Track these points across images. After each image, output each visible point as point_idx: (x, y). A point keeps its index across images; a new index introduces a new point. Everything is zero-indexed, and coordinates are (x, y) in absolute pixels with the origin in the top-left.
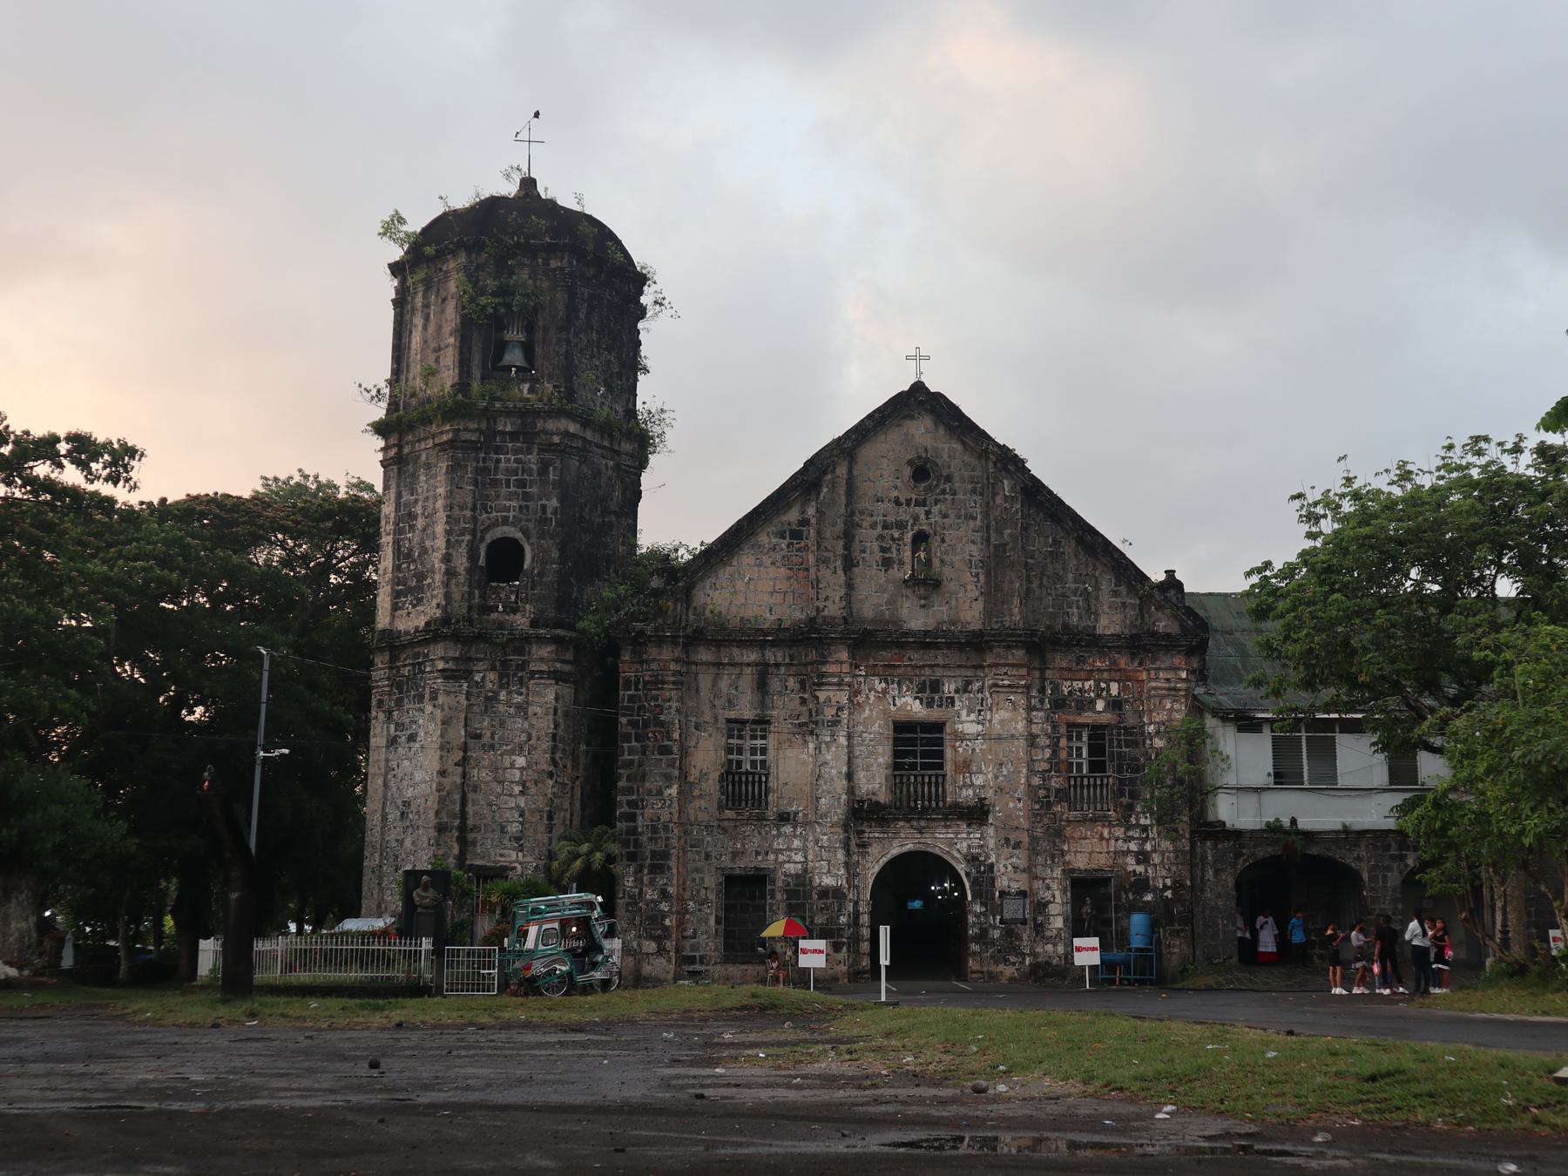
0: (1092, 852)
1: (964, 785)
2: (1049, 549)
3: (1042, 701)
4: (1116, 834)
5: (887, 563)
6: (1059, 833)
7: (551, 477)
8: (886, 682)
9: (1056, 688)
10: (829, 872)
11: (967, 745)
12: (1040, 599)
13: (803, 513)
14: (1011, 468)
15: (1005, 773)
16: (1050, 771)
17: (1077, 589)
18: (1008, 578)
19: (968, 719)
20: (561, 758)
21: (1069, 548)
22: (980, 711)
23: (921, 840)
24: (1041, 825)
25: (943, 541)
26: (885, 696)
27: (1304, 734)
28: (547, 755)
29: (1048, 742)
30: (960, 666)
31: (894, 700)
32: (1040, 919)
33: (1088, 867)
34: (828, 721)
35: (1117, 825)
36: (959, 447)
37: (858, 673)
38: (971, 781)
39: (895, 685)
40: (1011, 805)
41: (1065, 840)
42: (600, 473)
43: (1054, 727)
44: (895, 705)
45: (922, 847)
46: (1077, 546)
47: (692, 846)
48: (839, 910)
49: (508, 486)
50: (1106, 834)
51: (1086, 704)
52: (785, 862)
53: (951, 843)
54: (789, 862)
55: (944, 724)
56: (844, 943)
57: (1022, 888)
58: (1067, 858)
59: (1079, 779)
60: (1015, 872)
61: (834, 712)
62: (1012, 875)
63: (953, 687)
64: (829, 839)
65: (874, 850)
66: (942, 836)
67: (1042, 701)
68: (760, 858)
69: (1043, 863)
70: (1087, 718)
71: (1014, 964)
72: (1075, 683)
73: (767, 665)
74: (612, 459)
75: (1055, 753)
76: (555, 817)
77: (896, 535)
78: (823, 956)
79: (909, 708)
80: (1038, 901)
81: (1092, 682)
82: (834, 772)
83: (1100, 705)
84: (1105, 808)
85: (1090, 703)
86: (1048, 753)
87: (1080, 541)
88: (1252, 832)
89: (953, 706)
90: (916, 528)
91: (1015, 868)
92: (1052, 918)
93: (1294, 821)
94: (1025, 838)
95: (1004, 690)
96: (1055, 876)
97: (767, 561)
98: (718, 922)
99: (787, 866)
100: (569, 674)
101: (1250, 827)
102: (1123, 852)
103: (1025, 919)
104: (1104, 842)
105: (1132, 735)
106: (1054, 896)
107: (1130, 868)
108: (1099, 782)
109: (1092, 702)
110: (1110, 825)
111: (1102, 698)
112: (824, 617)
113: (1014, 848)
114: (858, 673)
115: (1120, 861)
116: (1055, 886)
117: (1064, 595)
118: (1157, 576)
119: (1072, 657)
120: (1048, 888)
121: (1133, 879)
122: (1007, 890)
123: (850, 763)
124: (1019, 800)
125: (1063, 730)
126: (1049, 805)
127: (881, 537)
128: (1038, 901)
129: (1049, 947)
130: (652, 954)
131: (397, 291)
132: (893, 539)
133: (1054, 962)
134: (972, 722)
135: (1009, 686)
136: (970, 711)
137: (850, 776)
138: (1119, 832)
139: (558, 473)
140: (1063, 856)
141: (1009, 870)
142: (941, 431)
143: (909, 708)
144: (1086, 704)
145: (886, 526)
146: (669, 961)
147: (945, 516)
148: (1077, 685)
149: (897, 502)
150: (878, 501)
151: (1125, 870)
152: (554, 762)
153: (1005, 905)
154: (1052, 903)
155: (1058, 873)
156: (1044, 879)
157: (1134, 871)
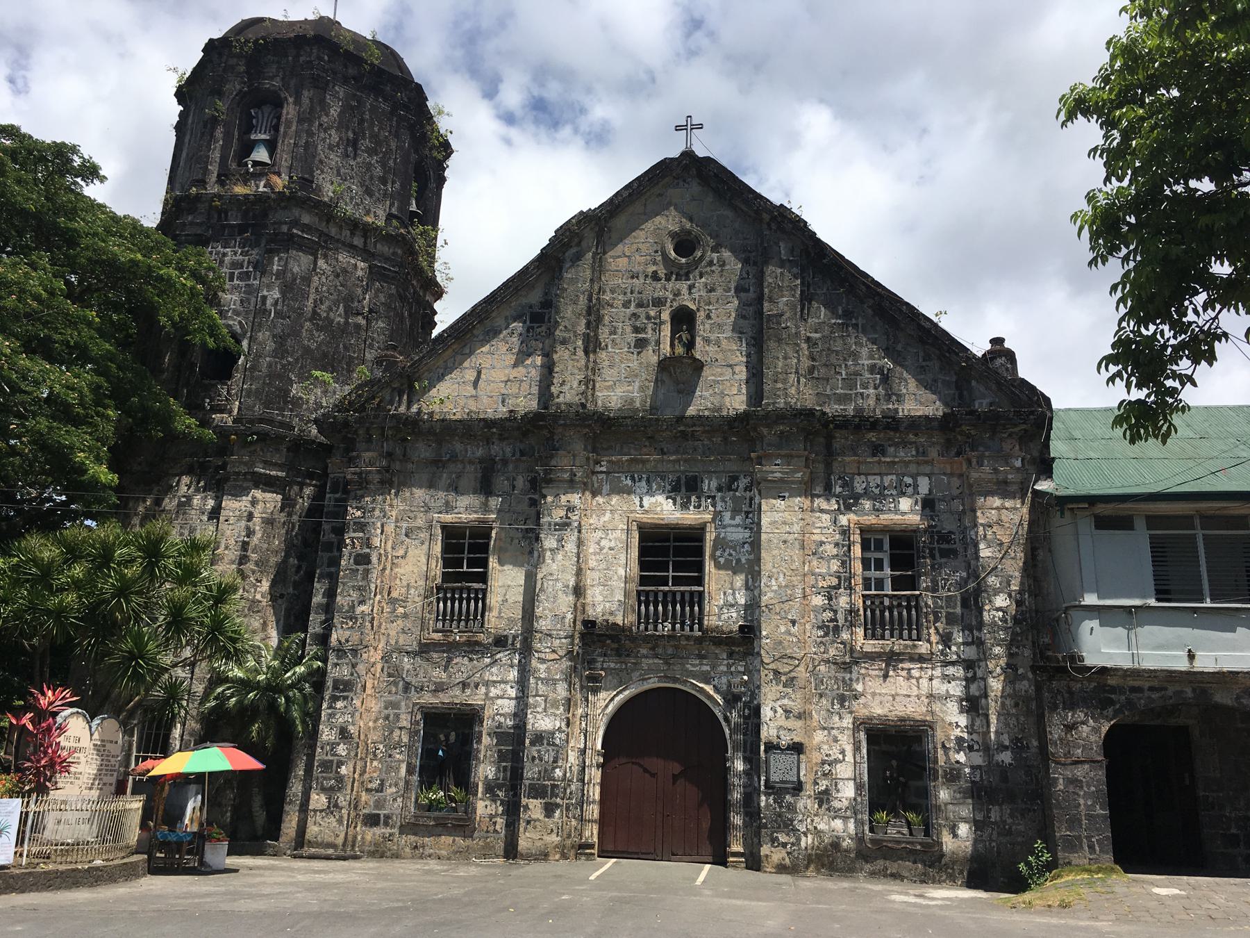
5: (641, 344)
7: (275, 267)
11: (730, 555)
13: (546, 294)
19: (733, 522)
22: (747, 513)
25: (708, 317)
27: (1200, 533)
28: (234, 566)
29: (835, 551)
34: (556, 524)
36: (729, 213)
37: (598, 469)
39: (644, 483)
44: (642, 506)
48: (555, 761)
49: (231, 279)
52: (498, 697)
54: (502, 697)
56: (558, 806)
57: (796, 739)
59: (914, 637)
60: (787, 718)
61: (563, 513)
62: (782, 721)
63: (714, 484)
64: (548, 668)
68: (468, 692)
72: (870, 478)
73: (492, 460)
77: (652, 313)
82: (559, 585)
84: (914, 637)
90: (675, 304)
91: (787, 712)
98: (410, 771)
99: (499, 702)
105: (948, 542)
106: (843, 752)
112: (558, 405)
114: (598, 469)
117: (857, 374)
118: (979, 346)
122: (775, 741)
123: (579, 572)
126: (837, 630)
127: (635, 316)
130: (321, 811)
131: (181, 114)
132: (648, 318)
133: (845, 844)
134: (737, 526)
136: (735, 512)
137: (578, 591)
139: (282, 263)
141: (778, 715)
142: (710, 199)
145: (640, 305)
146: (340, 821)
147: (712, 290)
150: (632, 277)
153: (772, 762)
155: (848, 721)
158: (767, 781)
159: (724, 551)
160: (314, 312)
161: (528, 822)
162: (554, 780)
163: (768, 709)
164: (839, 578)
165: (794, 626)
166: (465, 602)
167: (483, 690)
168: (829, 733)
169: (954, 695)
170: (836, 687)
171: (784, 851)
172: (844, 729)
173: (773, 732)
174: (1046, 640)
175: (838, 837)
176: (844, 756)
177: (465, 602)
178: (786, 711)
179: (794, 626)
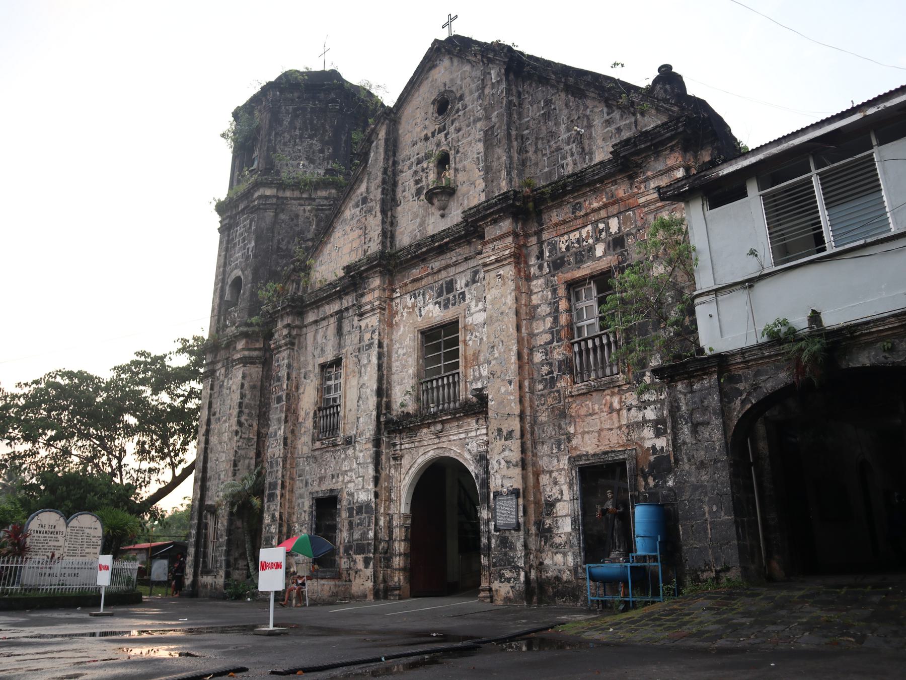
0: (601, 430)
1: (474, 379)
2: (542, 112)
3: (541, 267)
4: (628, 403)
6: (563, 414)
8: (415, 297)
9: (554, 247)
10: (363, 488)
12: (536, 164)
14: (491, 55)
15: (497, 355)
16: (551, 342)
17: (569, 138)
18: (496, 156)
20: (247, 420)
21: (560, 100)
23: (440, 445)
24: (544, 407)
26: (413, 310)
30: (466, 259)
31: (420, 310)
32: (548, 522)
33: (598, 450)
35: (628, 390)
38: (480, 373)
40: (503, 390)
41: (573, 420)
42: (297, 216)
43: (554, 291)
45: (440, 453)
46: (567, 96)
47: (299, 477)
50: (616, 405)
51: (584, 254)
53: (464, 444)
55: (457, 322)
57: (515, 487)
58: (574, 442)
59: (583, 343)
60: (508, 467)
62: (505, 471)
65: (405, 462)
66: (455, 438)
67: (541, 267)
69: (549, 452)
70: (586, 269)
71: (509, 580)
72: (572, 236)
74: (309, 205)
75: (556, 320)
76: (240, 464)
78: (281, 572)
79: (431, 315)
80: (546, 500)
81: (589, 228)
83: (600, 250)
85: (589, 251)
86: (549, 322)
87: (568, 89)
88: (743, 352)
89: (464, 300)
92: (560, 520)
93: (815, 317)
94: (516, 425)
95: (492, 267)
96: (562, 466)
97: (348, 228)
100: (257, 358)
101: (742, 344)
102: (637, 423)
103: (518, 524)
104: (615, 415)
106: (561, 493)
107: (648, 444)
108: (605, 341)
109: (591, 249)
110: (621, 392)
111: (602, 241)
113: (506, 439)
115: (635, 436)
116: (562, 479)
119: (568, 209)
120: (556, 483)
121: (652, 458)
122: (500, 489)
124: (510, 382)
125: (562, 292)
126: (553, 381)
128: (546, 500)
129: (559, 558)
135: (497, 261)
138: (631, 398)
140: (569, 440)
141: (502, 466)
143: (431, 315)
144: (584, 254)
148: (575, 236)
149: (426, 138)
151: (641, 447)
152: (240, 424)
154: (559, 500)
155: (564, 462)
156: (551, 472)
157: (654, 447)
158: (495, 525)
159: (472, 335)
160: (278, 248)
161: (356, 572)
162: (369, 540)
163: (495, 462)
164: (552, 333)
165: (510, 385)
166: (441, 389)
167: (341, 479)
168: (550, 476)
169: (650, 421)
170: (553, 433)
171: (509, 585)
172: (561, 470)
173: (499, 482)
174: (563, 384)
175: (560, 571)
176: (562, 495)
177: (441, 389)
178: (507, 462)
179: (510, 385)
